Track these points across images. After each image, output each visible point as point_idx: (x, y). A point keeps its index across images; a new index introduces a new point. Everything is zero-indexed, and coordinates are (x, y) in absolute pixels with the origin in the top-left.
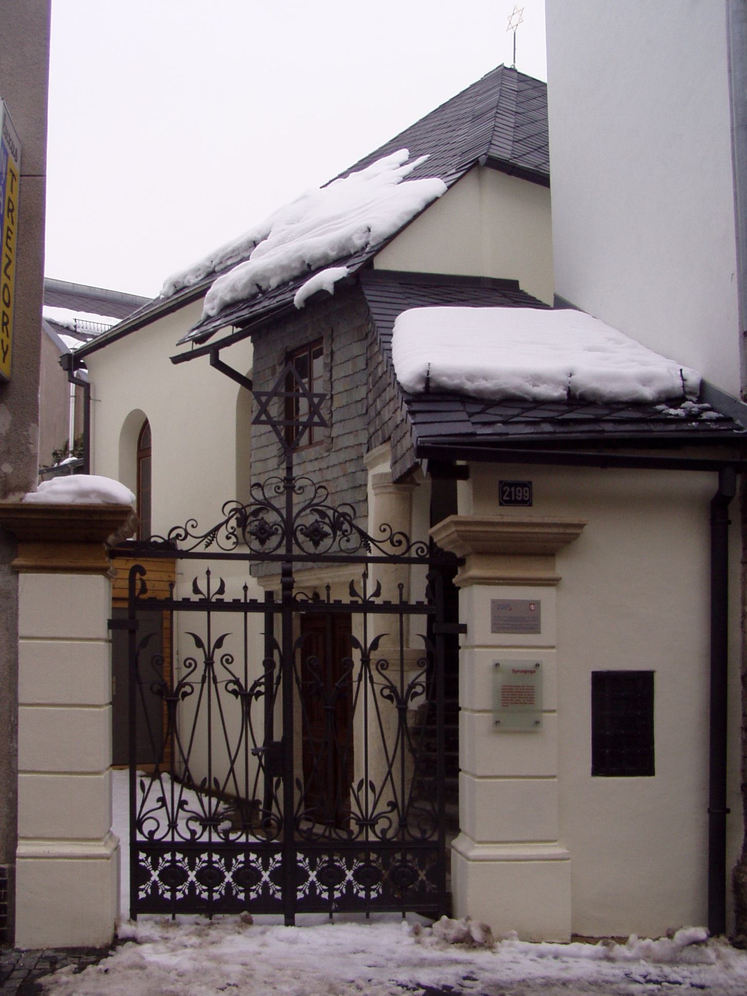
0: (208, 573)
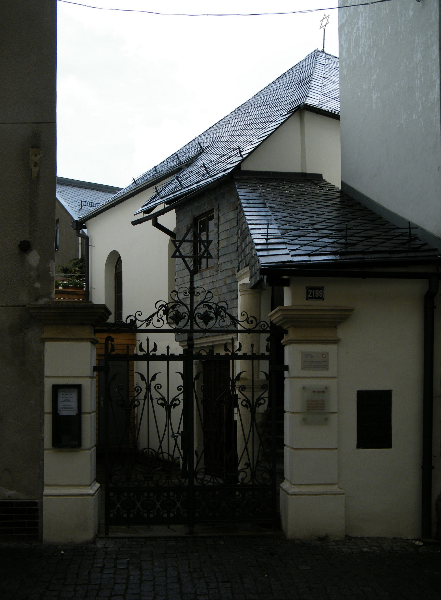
0: (148, 340)
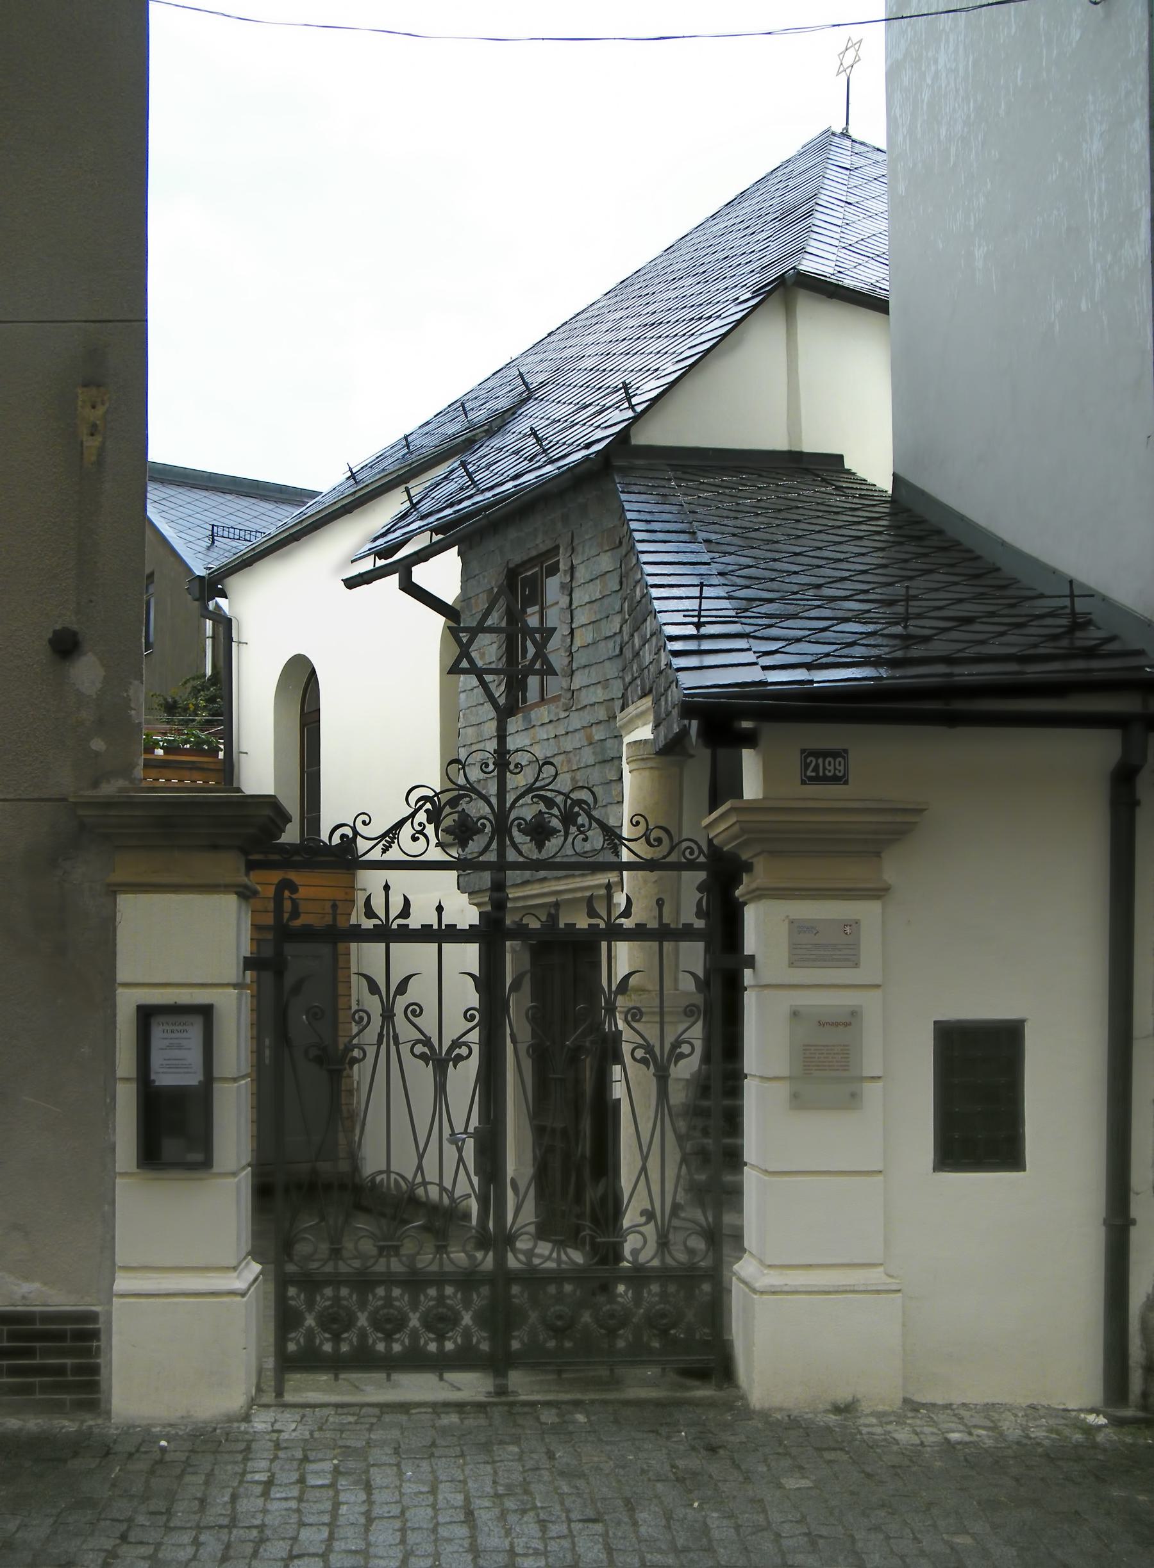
0: (387, 888)
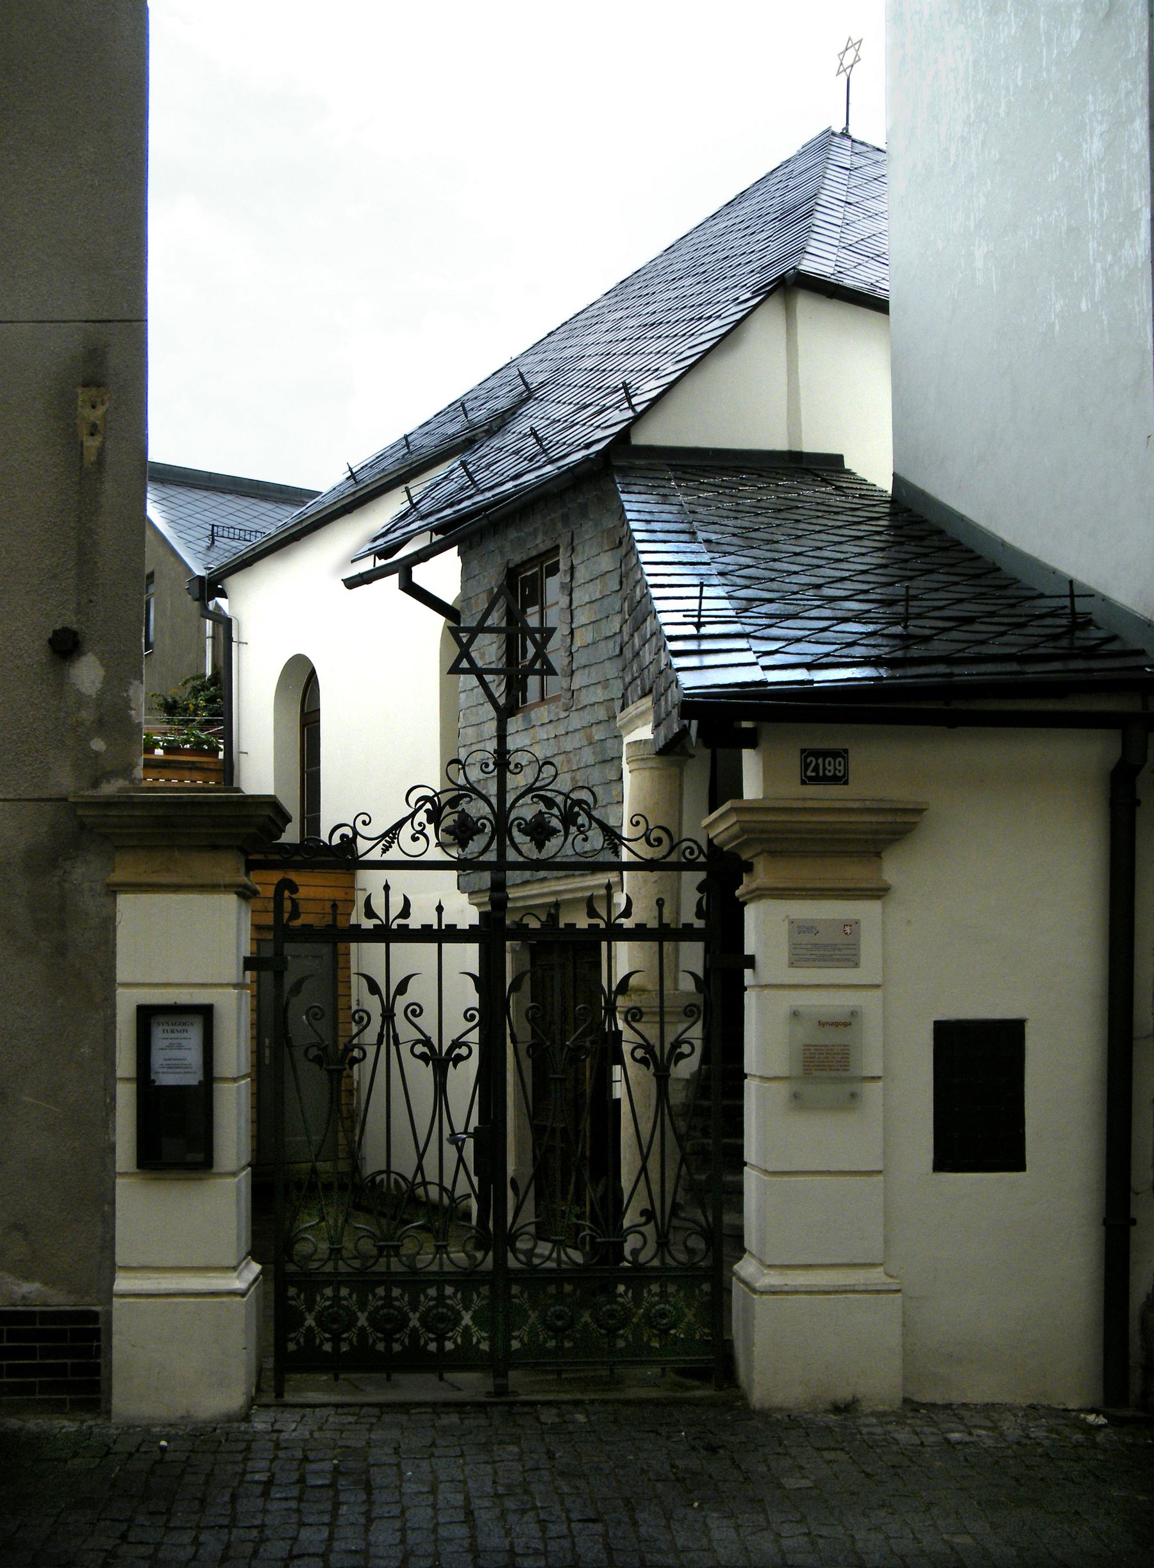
0: (387, 888)
